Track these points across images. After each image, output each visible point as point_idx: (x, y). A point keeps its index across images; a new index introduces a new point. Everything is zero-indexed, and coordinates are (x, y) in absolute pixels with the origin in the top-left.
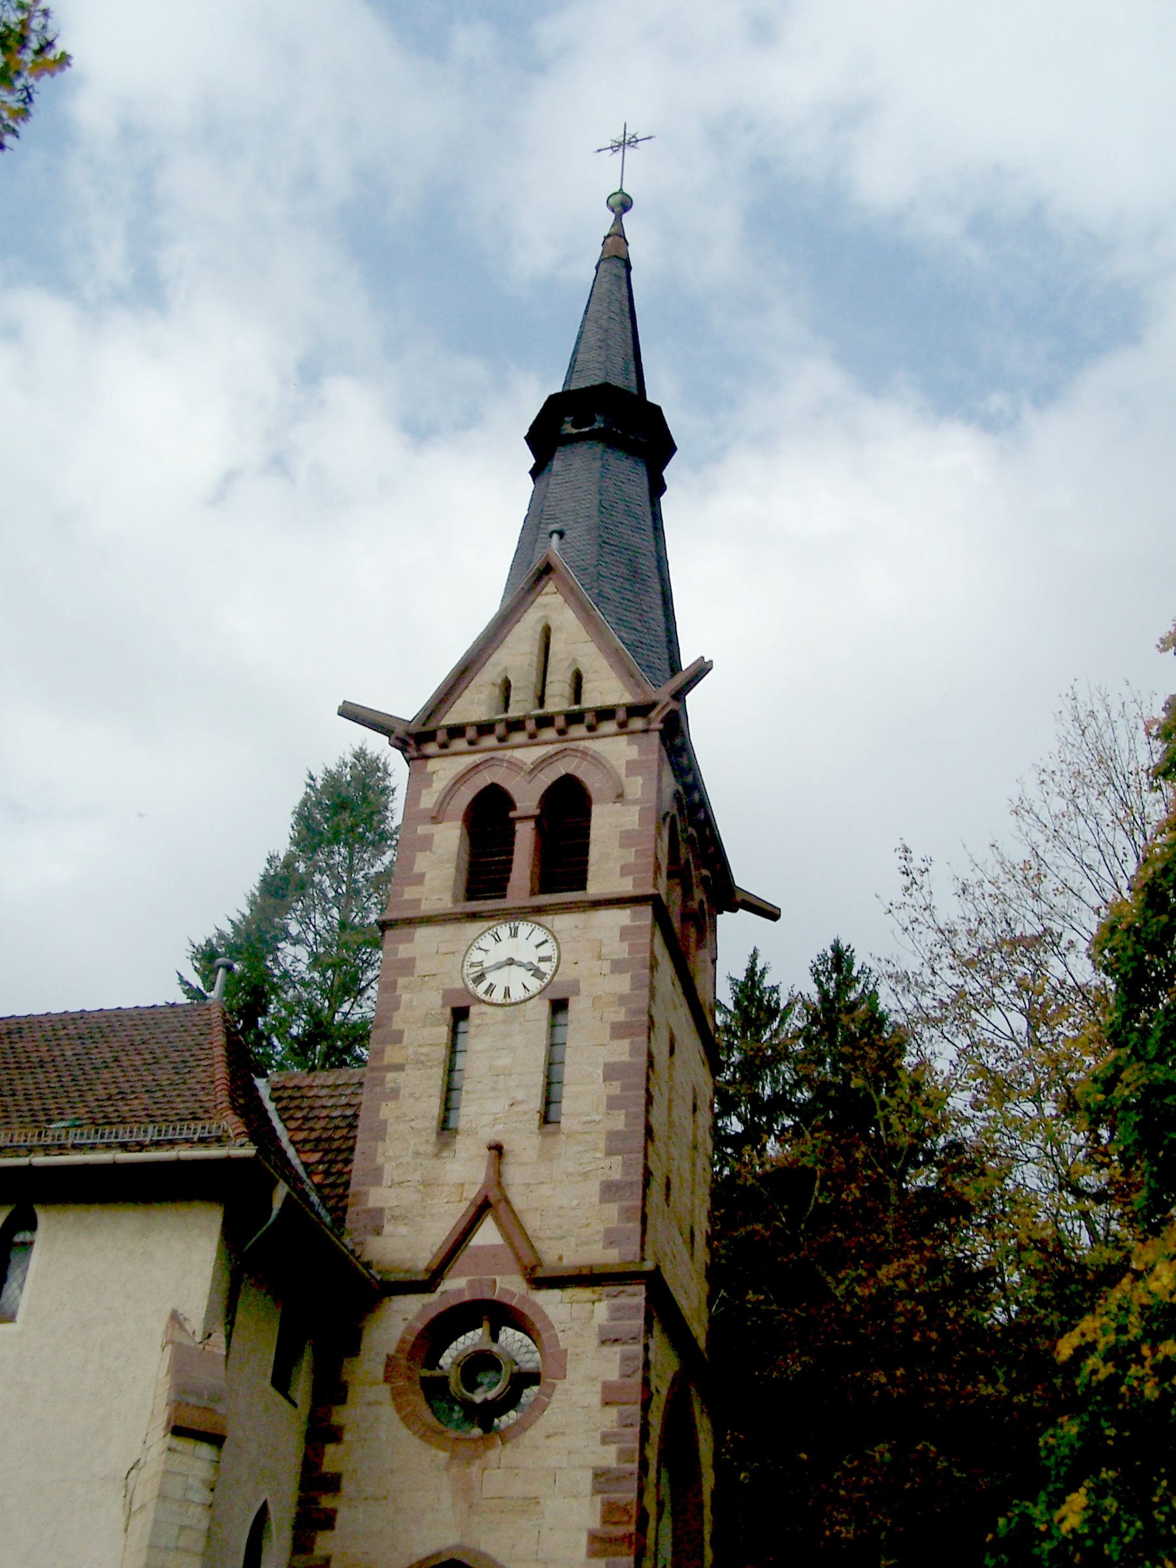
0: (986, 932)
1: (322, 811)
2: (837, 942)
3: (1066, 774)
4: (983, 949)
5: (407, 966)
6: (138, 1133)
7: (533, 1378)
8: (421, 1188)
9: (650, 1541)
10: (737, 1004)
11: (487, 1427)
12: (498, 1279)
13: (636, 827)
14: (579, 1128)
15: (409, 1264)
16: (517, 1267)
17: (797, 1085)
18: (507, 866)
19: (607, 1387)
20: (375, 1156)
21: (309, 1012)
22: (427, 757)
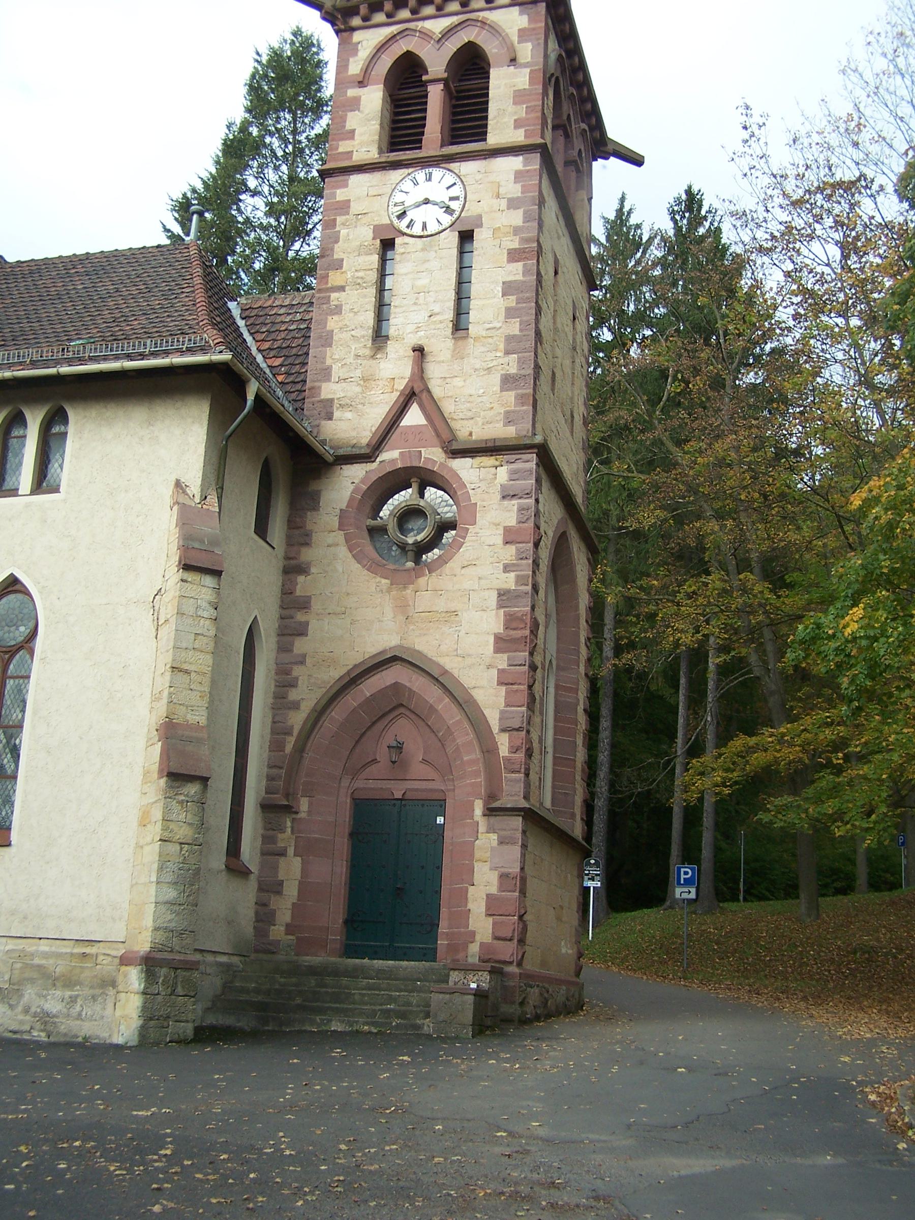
0: (811, 176)
1: (269, 83)
2: (690, 187)
3: (890, 34)
4: (808, 191)
5: (344, 207)
6: (139, 345)
7: (451, 525)
8: (362, 382)
9: (540, 642)
10: (608, 238)
11: (417, 560)
12: (423, 450)
13: (527, 87)
14: (484, 333)
15: (355, 441)
16: (435, 440)
17: (655, 304)
18: (421, 123)
19: (507, 530)
20: (324, 358)
21: (268, 250)
22: (353, 29)
